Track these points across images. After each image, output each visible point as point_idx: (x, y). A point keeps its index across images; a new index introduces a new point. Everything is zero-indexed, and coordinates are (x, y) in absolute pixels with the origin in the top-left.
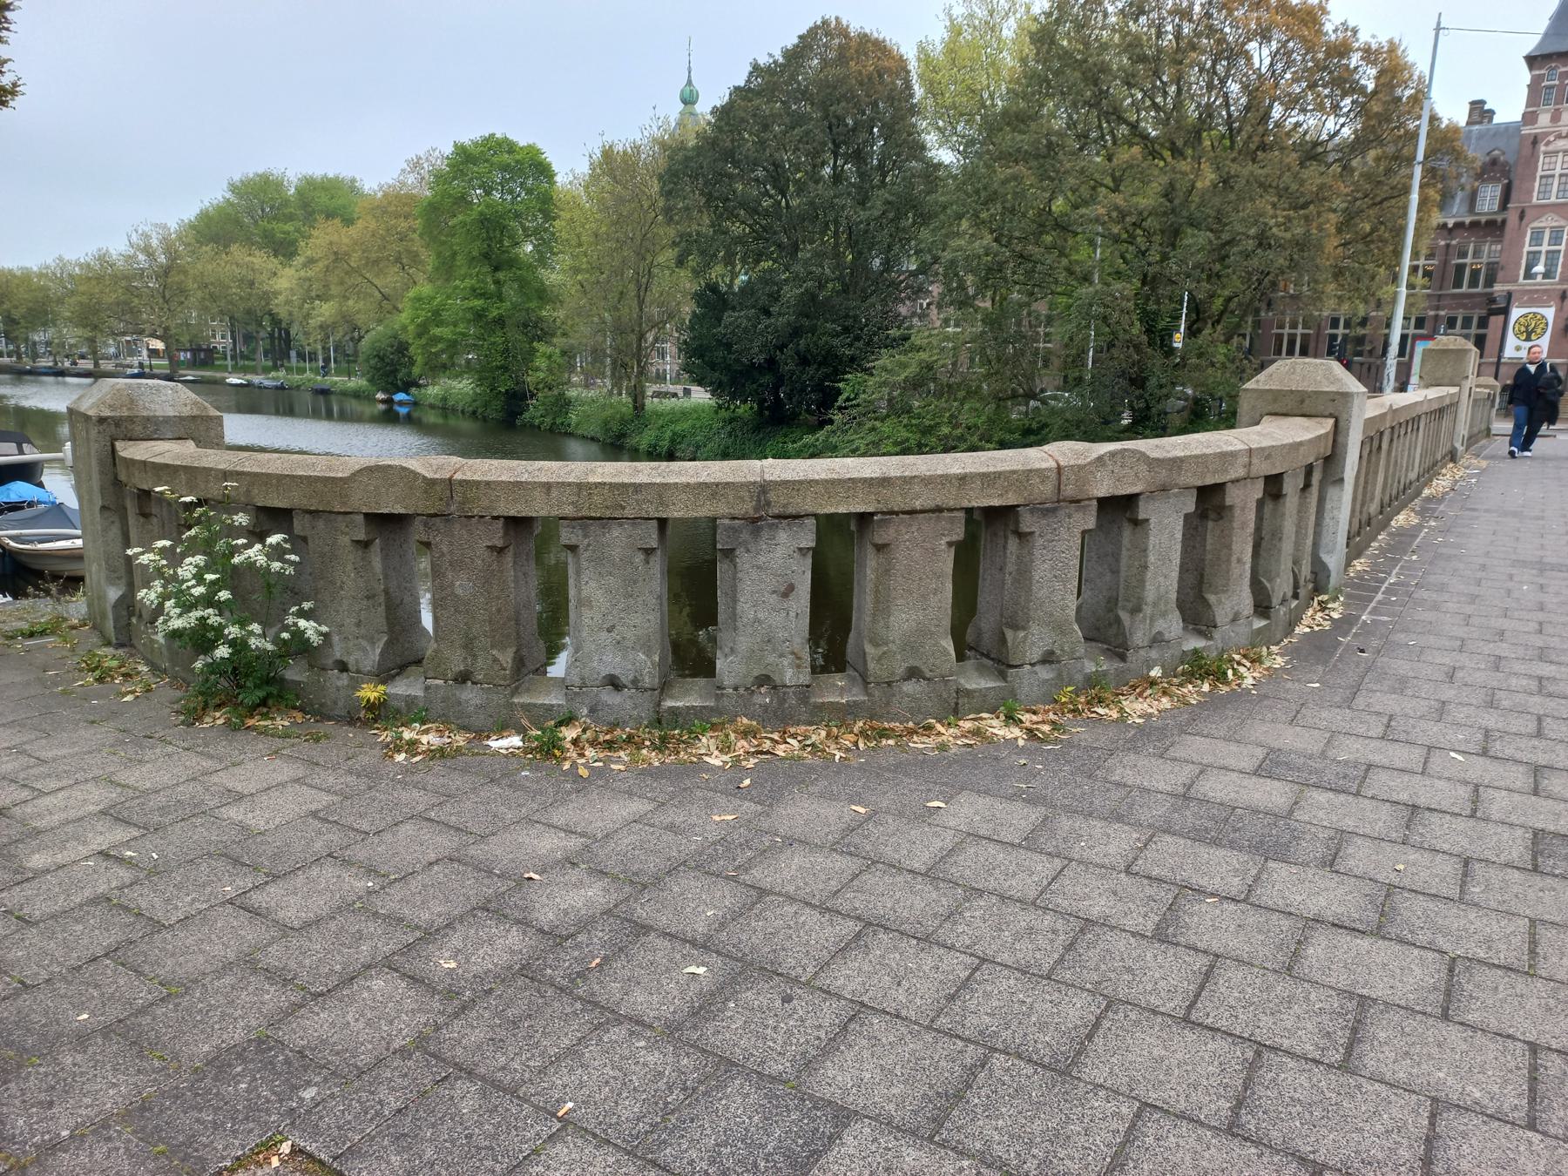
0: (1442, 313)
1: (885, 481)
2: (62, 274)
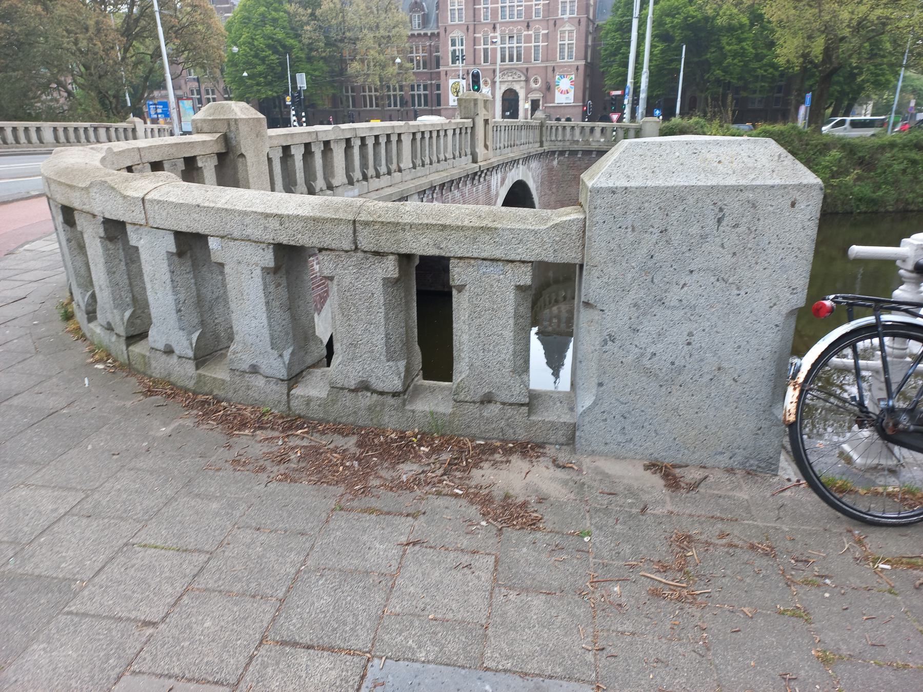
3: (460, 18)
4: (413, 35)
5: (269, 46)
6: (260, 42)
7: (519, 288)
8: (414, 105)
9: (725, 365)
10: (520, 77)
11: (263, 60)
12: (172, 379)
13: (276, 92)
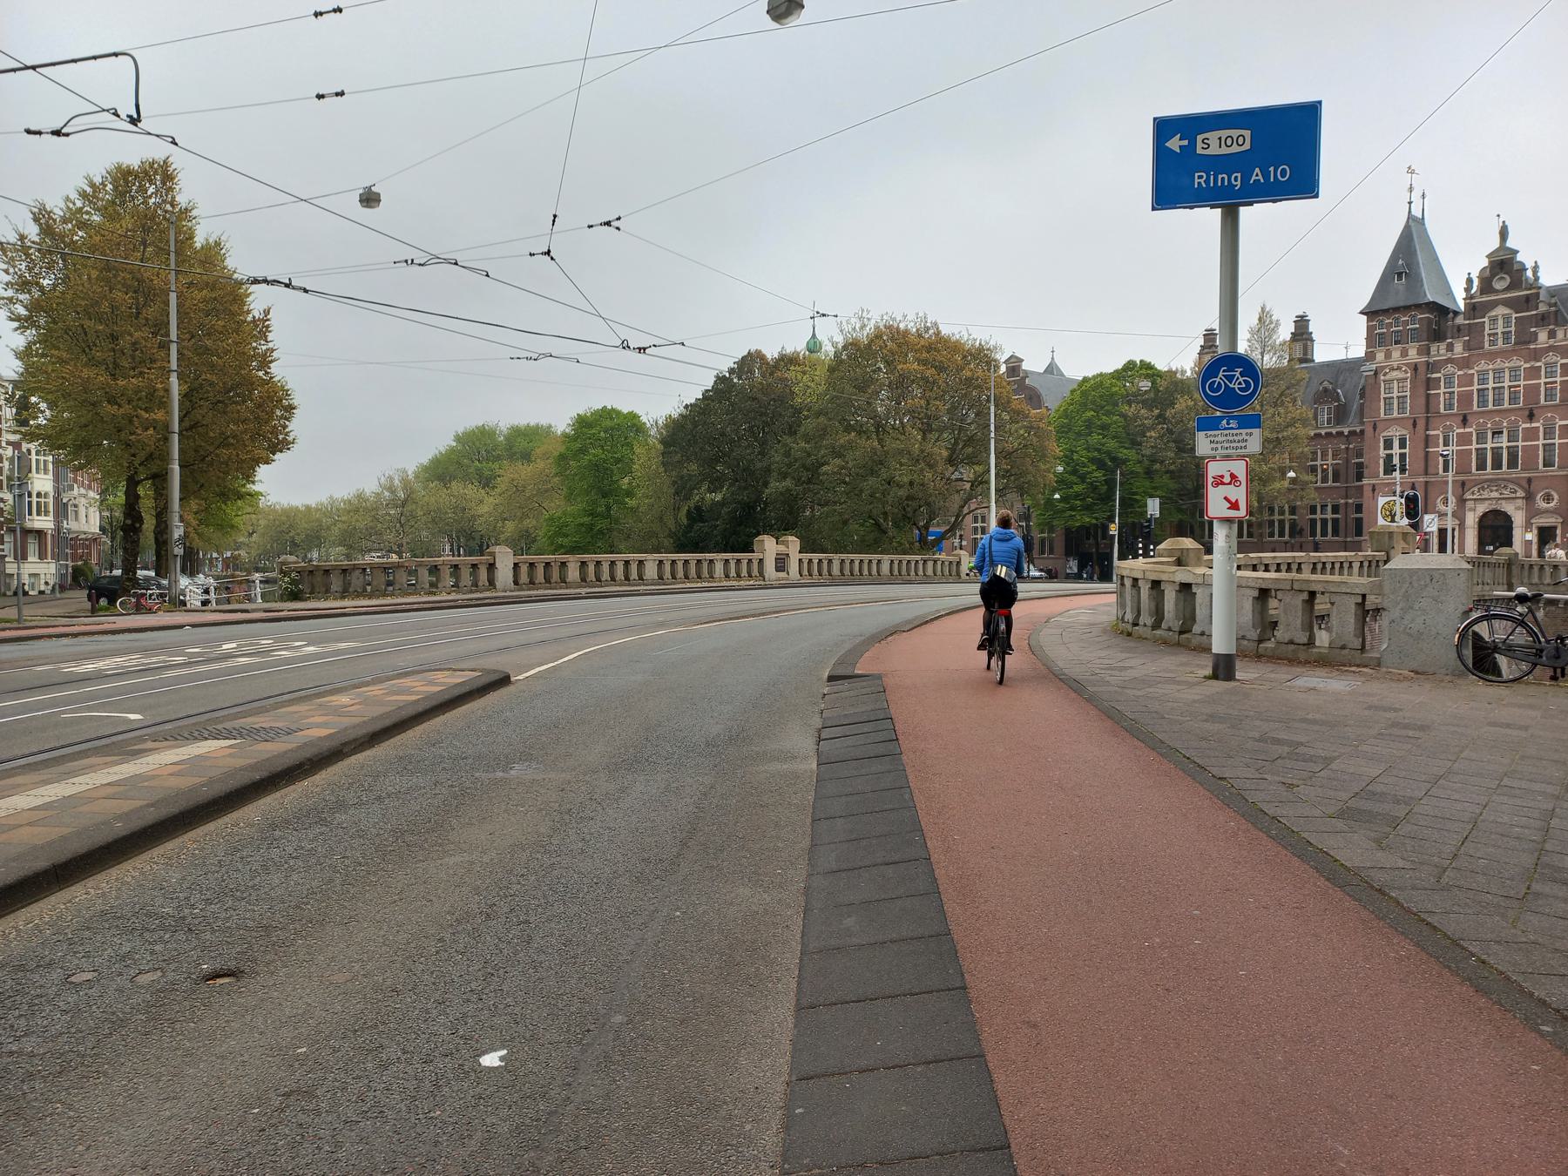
0: (1350, 501)
2: (331, 509)
3: (1401, 409)
4: (1318, 436)
5: (1092, 460)
6: (1081, 456)
7: (1356, 603)
8: (1313, 534)
9: (1440, 632)
10: (1516, 492)
11: (1083, 478)
12: (1203, 646)
13: (1097, 519)
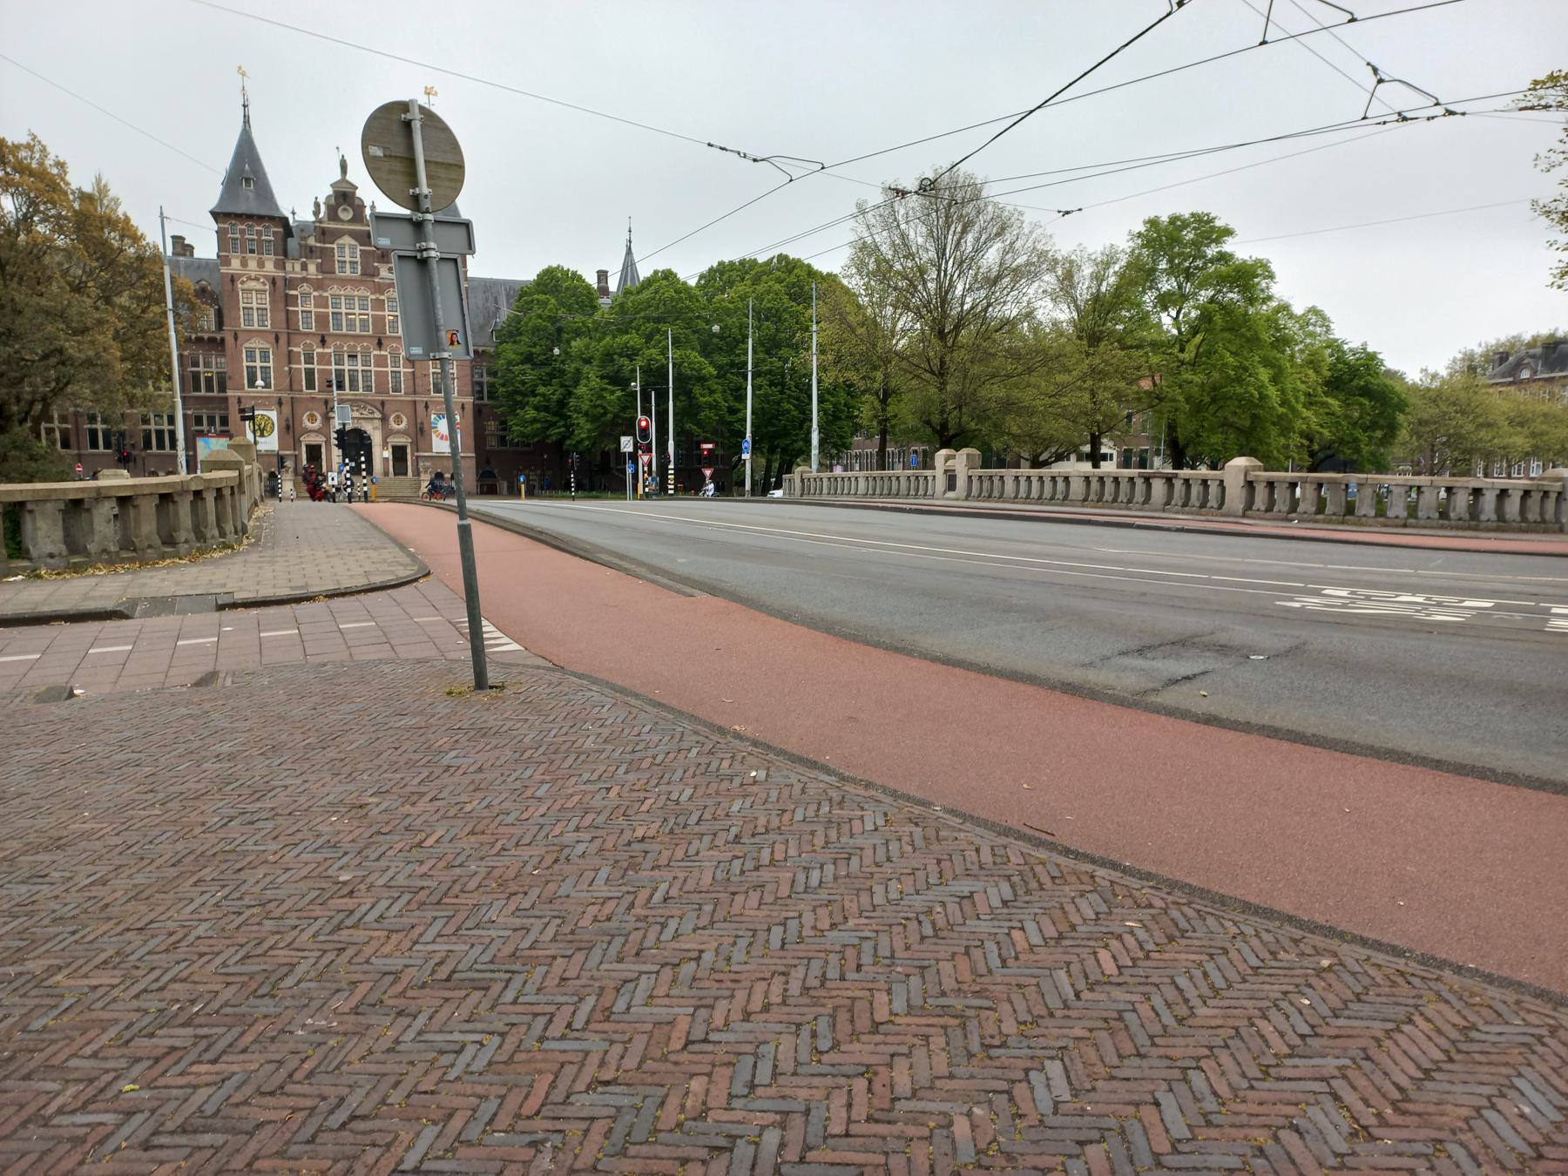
1: (135, 486)
